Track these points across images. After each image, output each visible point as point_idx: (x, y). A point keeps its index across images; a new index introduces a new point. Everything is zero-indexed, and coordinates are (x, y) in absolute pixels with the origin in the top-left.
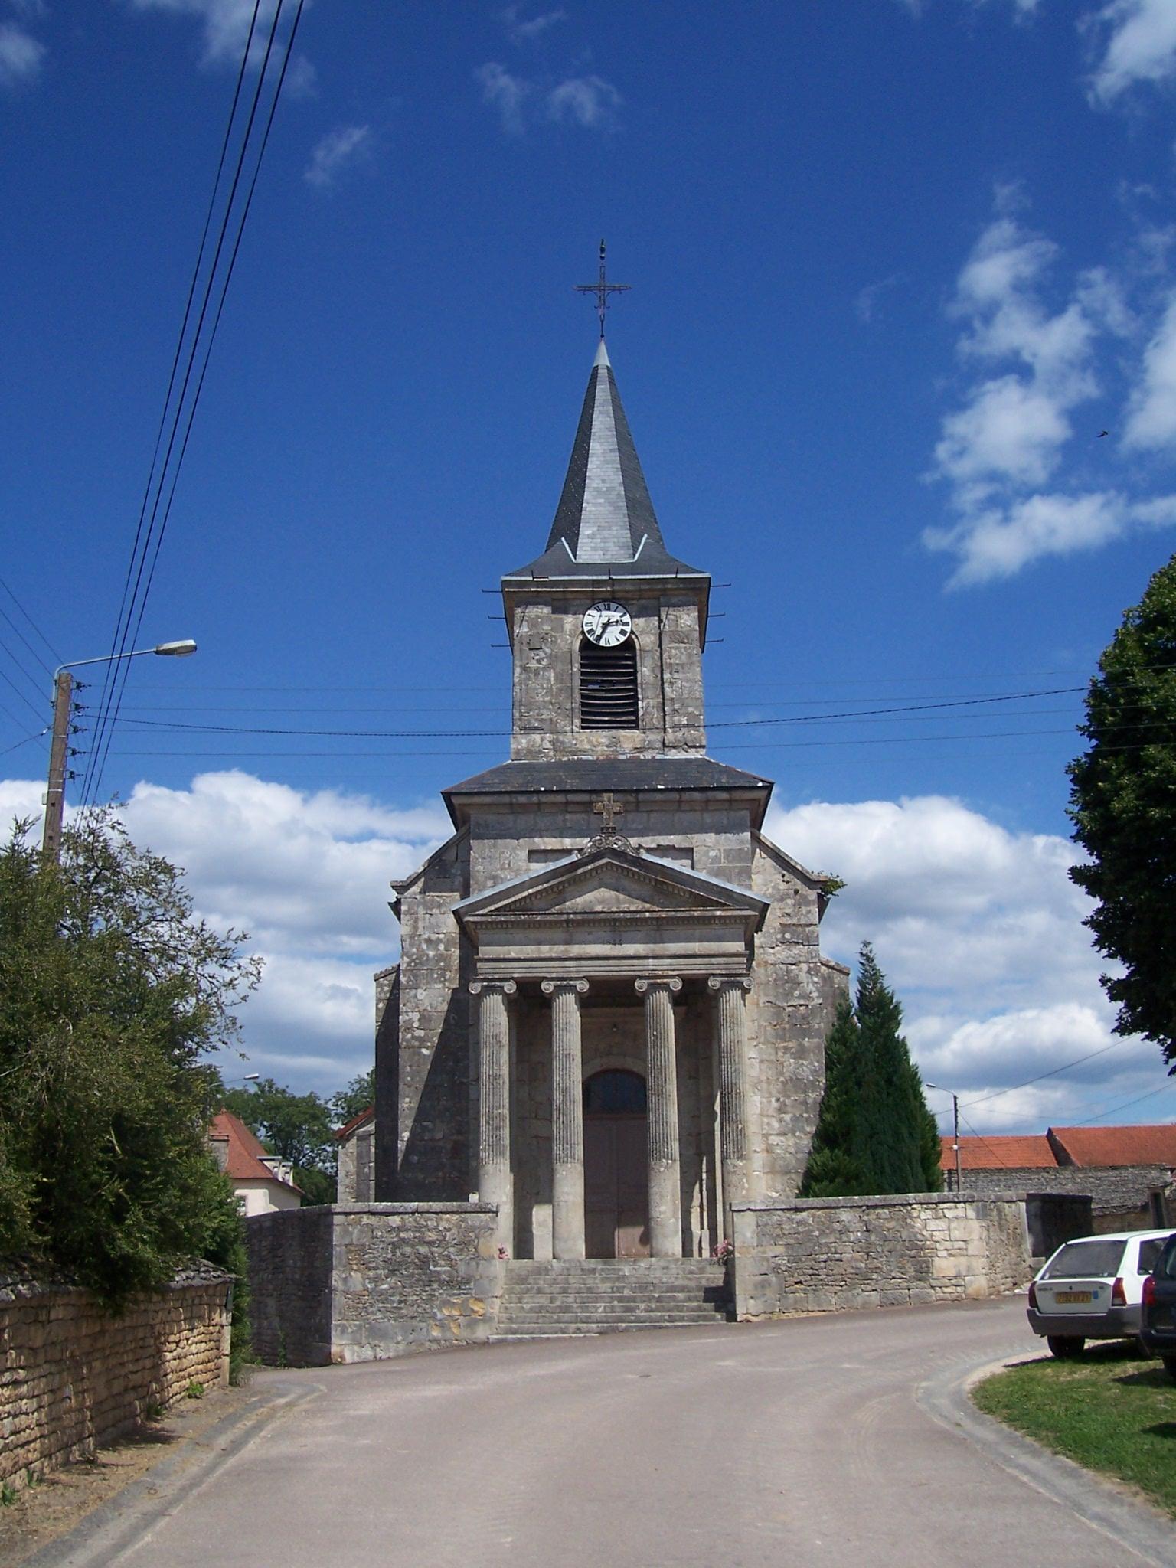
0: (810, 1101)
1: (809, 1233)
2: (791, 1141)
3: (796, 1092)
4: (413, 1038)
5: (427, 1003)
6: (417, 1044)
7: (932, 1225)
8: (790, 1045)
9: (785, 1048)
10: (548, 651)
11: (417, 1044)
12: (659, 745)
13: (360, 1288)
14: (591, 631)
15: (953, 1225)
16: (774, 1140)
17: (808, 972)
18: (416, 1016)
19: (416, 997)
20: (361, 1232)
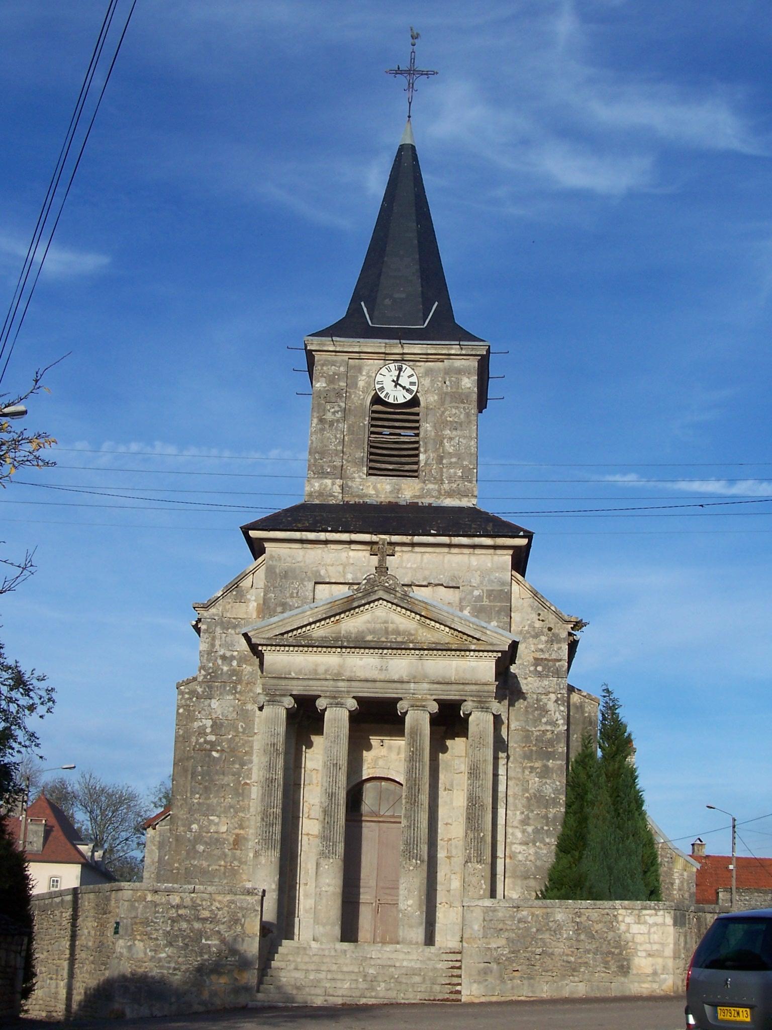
0: (550, 815)
1: (527, 929)
2: (532, 851)
3: (539, 807)
4: (206, 742)
5: (219, 712)
6: (208, 747)
7: (635, 929)
8: (537, 765)
9: (531, 768)
10: (343, 405)
11: (208, 747)
12: (435, 493)
13: (141, 955)
14: (382, 389)
15: (652, 930)
16: (517, 848)
17: (556, 701)
18: (209, 723)
19: (210, 706)
20: (145, 907)
